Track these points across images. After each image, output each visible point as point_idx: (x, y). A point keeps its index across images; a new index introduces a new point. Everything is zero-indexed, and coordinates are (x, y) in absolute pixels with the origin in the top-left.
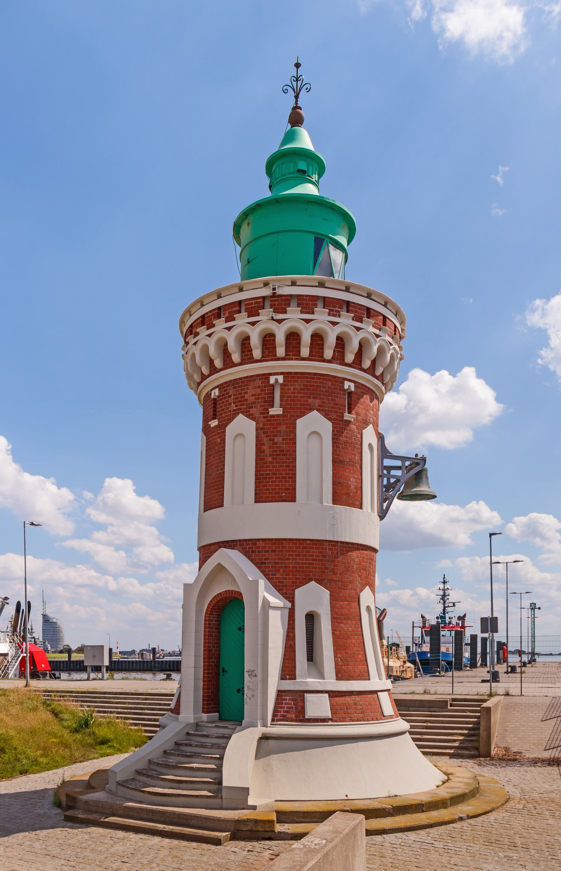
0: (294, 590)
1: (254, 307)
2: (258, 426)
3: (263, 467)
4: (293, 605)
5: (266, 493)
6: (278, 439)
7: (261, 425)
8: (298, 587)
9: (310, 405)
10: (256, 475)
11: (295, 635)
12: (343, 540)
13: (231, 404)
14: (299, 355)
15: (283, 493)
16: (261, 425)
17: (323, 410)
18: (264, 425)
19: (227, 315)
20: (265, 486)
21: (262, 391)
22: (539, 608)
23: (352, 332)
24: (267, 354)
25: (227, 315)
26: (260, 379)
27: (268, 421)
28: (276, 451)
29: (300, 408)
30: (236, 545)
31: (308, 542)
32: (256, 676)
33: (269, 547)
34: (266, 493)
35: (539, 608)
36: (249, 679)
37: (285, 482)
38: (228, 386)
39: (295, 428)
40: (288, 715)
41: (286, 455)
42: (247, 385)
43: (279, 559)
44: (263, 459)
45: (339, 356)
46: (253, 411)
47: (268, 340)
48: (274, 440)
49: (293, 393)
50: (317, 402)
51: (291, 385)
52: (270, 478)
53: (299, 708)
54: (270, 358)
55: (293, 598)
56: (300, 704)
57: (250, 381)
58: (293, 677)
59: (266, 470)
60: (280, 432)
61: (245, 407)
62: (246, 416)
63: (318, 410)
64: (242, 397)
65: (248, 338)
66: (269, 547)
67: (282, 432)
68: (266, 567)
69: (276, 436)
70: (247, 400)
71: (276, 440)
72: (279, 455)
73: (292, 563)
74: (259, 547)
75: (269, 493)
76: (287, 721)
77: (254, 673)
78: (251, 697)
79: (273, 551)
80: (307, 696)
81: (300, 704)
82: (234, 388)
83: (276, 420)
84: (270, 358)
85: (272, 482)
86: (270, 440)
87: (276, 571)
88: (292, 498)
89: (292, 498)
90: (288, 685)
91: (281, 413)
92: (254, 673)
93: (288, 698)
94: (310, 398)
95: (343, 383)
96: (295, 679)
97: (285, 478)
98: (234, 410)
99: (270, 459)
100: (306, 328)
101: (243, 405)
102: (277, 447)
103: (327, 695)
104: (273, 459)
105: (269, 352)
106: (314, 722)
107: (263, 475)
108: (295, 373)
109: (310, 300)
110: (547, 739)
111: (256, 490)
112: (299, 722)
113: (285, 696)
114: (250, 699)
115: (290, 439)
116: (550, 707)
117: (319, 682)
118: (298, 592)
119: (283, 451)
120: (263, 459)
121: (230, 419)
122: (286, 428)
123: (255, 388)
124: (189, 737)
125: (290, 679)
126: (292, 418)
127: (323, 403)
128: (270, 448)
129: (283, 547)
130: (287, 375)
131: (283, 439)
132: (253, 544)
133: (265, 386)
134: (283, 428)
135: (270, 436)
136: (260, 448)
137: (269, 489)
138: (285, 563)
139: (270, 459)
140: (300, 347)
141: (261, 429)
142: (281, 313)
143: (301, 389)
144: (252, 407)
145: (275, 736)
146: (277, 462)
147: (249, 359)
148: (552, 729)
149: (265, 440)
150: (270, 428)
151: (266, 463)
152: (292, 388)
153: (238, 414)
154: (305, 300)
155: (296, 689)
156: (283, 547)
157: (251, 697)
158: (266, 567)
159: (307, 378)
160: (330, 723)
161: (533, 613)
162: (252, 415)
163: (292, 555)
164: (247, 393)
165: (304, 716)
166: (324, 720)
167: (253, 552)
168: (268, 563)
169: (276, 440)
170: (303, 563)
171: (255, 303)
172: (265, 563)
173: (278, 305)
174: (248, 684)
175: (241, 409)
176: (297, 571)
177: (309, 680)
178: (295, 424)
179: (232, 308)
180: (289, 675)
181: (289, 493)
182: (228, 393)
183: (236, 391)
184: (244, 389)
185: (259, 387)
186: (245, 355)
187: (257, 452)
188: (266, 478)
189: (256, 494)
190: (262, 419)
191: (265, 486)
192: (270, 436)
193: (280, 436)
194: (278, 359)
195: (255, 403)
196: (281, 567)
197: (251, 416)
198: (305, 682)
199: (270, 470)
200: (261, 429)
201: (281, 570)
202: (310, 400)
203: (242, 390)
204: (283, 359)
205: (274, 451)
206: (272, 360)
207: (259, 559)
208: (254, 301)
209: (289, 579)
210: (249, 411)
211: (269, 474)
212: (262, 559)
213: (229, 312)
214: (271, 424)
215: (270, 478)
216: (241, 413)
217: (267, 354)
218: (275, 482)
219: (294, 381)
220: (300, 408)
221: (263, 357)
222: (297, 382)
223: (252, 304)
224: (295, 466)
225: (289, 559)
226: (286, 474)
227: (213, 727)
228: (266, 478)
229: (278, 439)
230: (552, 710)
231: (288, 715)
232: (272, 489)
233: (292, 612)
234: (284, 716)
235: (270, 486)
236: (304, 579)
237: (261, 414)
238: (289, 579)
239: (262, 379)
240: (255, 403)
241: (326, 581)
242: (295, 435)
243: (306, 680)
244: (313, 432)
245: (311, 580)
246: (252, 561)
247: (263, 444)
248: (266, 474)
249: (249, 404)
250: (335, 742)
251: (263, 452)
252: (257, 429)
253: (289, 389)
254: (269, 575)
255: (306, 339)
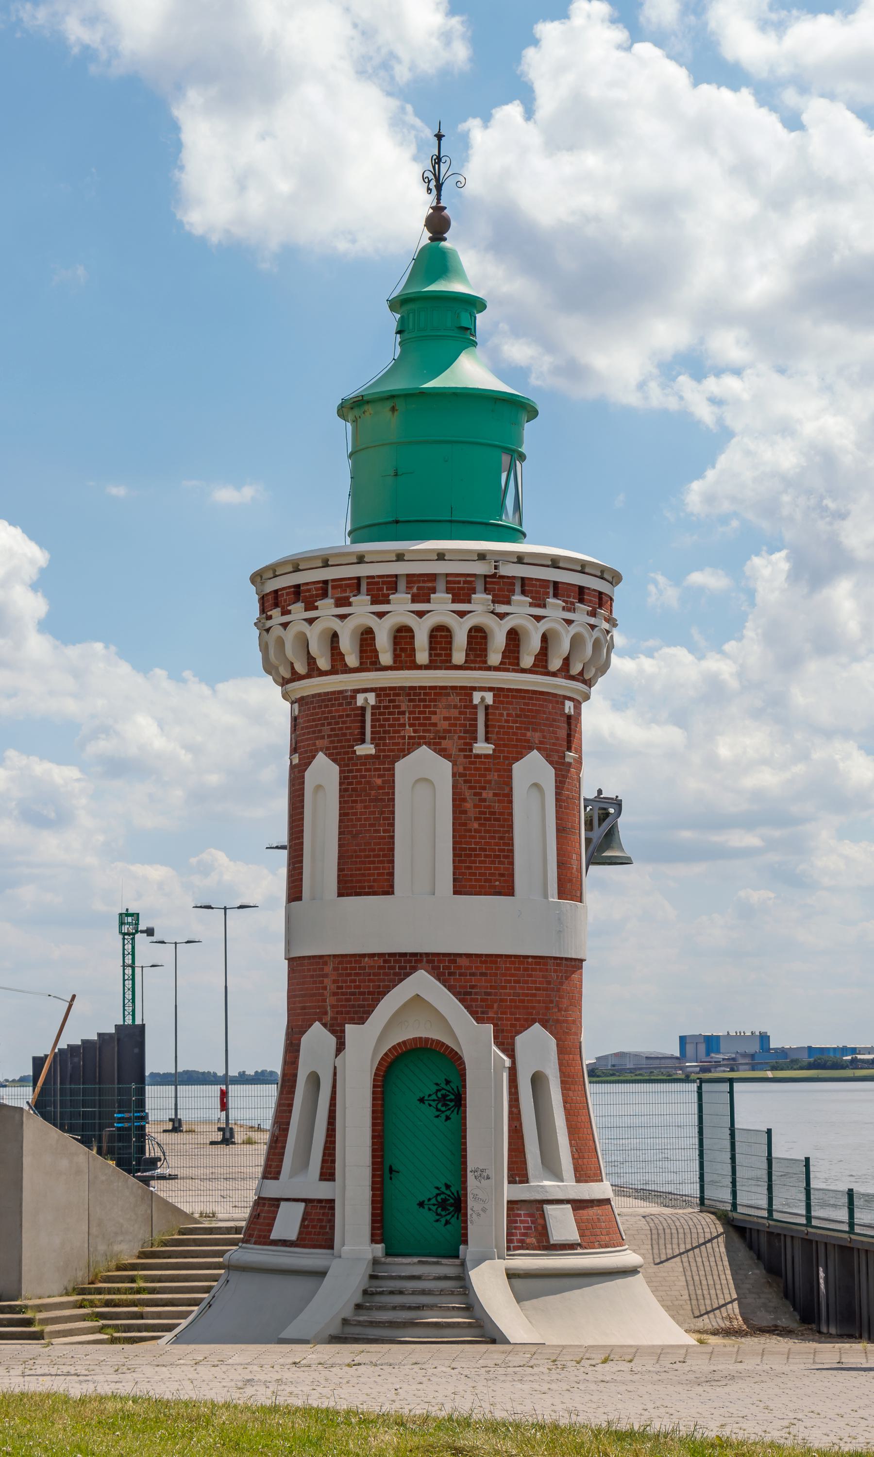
0: (513, 1038)
1: (463, 589)
2: (455, 770)
3: (465, 837)
4: (514, 1062)
5: (471, 880)
6: (487, 794)
7: (461, 770)
8: (519, 1032)
9: (528, 741)
10: (454, 849)
11: (519, 1111)
12: (569, 956)
13: (404, 725)
14: (518, 664)
15: (496, 880)
16: (461, 770)
17: (545, 749)
18: (465, 769)
19: (415, 590)
20: (470, 868)
21: (460, 713)
22: (150, 932)
23: (560, 627)
24: (472, 658)
25: (415, 590)
26: (458, 694)
27: (471, 763)
28: (485, 813)
29: (516, 746)
30: (421, 961)
31: (530, 960)
32: (488, 1178)
33: (477, 968)
34: (471, 880)
35: (150, 932)
36: (477, 1183)
37: (500, 863)
38: (398, 695)
39: (511, 777)
40: (529, 1240)
41: (498, 820)
42: (435, 700)
43: (491, 987)
44: (465, 824)
45: (541, 664)
46: (445, 743)
47: (478, 638)
48: (480, 794)
49: (507, 721)
50: (536, 737)
51: (504, 709)
52: (476, 856)
53: (540, 1228)
54: (477, 665)
55: (513, 1050)
56: (540, 1221)
57: (440, 694)
58: (525, 1180)
59: (470, 843)
60: (489, 782)
61: (432, 735)
62: (435, 750)
63: (539, 749)
64: (425, 719)
65: (335, 636)
66: (477, 968)
67: (493, 782)
68: (472, 1000)
69: (484, 788)
70: (435, 725)
71: (485, 794)
72: (489, 819)
73: (510, 995)
74: (460, 967)
75: (476, 880)
76: (527, 1249)
77: (485, 1174)
78: (481, 1212)
79: (482, 974)
80: (548, 1208)
81: (540, 1221)
82: (410, 701)
83: (484, 763)
84: (477, 665)
85: (480, 862)
86: (475, 794)
87: (488, 1007)
88: (508, 890)
89: (508, 890)
90: (521, 1192)
91: (491, 752)
92: (485, 1174)
93: (522, 1212)
94: (528, 729)
95: (563, 704)
96: (527, 1182)
97: (498, 856)
98: (410, 738)
99: (476, 825)
100: (537, 629)
101: (429, 731)
102: (485, 807)
103: (569, 1206)
104: (480, 825)
105: (476, 656)
106: (562, 1250)
107: (465, 849)
108: (509, 690)
109: (540, 586)
110: (686, 1297)
111: (454, 874)
112: (543, 1250)
113: (518, 1209)
114: (479, 1215)
115: (505, 795)
116: (655, 1237)
117: (558, 1186)
118: (519, 1039)
119: (494, 813)
120: (465, 824)
121: (403, 750)
122: (499, 776)
123: (449, 707)
124: (376, 1283)
125: (521, 1182)
126: (507, 762)
127: (544, 737)
128: (475, 806)
129: (497, 968)
130: (498, 692)
131: (495, 795)
132: (450, 962)
133: (466, 707)
134: (493, 776)
135: (475, 788)
136: (460, 806)
137: (475, 874)
138: (501, 994)
139: (476, 825)
140: (451, 649)
141: (461, 775)
142: (503, 603)
143: (517, 716)
144: (444, 738)
145: (522, 1272)
146: (486, 831)
147: (442, 661)
148: (683, 1278)
149: (468, 794)
150: (475, 775)
151: (470, 831)
152: (505, 713)
153: (420, 745)
154: (535, 586)
155: (532, 1198)
156: (497, 968)
157: (481, 1212)
158: (472, 1000)
159: (524, 698)
160: (579, 1251)
161: (129, 947)
162: (445, 750)
163: (509, 982)
164: (435, 713)
165: (548, 1240)
166: (572, 1246)
167: (450, 974)
168: (476, 994)
169: (485, 794)
170: (524, 995)
171: (465, 582)
172: (470, 993)
173: (499, 590)
174: (475, 1192)
175: (424, 738)
176: (517, 1007)
177: (546, 1183)
178: (511, 770)
179: (424, 582)
180: (519, 1176)
181: (505, 881)
182: (398, 707)
183: (415, 707)
184: (429, 707)
185: (455, 707)
186: (436, 655)
187: (454, 812)
188: (470, 856)
189: (455, 880)
190: (461, 760)
191: (470, 868)
192: (475, 788)
193: (491, 789)
194: (489, 668)
195: (449, 731)
196: (495, 1001)
197: (443, 753)
198: (542, 1187)
199: (476, 843)
200: (461, 775)
201: (496, 1005)
202: (529, 734)
203: (425, 707)
204: (496, 669)
205: (481, 813)
206: (480, 669)
207: (460, 987)
208: (462, 579)
209: (507, 1019)
210: (439, 744)
211: (474, 850)
212: (465, 987)
213: (306, 596)
214: (476, 769)
215: (476, 856)
216: (425, 743)
217: (472, 658)
218: (484, 862)
219: (508, 703)
220: (516, 746)
221: (466, 662)
222: (511, 703)
223: (459, 582)
224: (512, 839)
225: (505, 988)
226: (500, 850)
227: (414, 1264)
228: (470, 856)
229: (487, 794)
230: (662, 1242)
231: (529, 1240)
232: (480, 874)
233: (513, 1072)
234: (522, 1241)
235: (477, 868)
236: (526, 1020)
237: (461, 750)
238: (507, 1019)
239: (460, 694)
240: (449, 731)
241: (551, 1023)
242: (511, 789)
243: (542, 1185)
244: (424, 783)
245: (533, 1021)
246: (450, 988)
247: (464, 800)
248: (471, 849)
249: (438, 731)
250: (566, 1281)
251: (465, 812)
252: (454, 775)
253: (501, 715)
254: (477, 1012)
255: (460, 640)
